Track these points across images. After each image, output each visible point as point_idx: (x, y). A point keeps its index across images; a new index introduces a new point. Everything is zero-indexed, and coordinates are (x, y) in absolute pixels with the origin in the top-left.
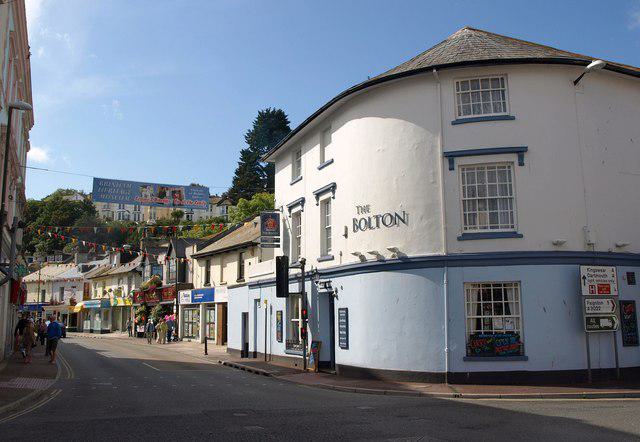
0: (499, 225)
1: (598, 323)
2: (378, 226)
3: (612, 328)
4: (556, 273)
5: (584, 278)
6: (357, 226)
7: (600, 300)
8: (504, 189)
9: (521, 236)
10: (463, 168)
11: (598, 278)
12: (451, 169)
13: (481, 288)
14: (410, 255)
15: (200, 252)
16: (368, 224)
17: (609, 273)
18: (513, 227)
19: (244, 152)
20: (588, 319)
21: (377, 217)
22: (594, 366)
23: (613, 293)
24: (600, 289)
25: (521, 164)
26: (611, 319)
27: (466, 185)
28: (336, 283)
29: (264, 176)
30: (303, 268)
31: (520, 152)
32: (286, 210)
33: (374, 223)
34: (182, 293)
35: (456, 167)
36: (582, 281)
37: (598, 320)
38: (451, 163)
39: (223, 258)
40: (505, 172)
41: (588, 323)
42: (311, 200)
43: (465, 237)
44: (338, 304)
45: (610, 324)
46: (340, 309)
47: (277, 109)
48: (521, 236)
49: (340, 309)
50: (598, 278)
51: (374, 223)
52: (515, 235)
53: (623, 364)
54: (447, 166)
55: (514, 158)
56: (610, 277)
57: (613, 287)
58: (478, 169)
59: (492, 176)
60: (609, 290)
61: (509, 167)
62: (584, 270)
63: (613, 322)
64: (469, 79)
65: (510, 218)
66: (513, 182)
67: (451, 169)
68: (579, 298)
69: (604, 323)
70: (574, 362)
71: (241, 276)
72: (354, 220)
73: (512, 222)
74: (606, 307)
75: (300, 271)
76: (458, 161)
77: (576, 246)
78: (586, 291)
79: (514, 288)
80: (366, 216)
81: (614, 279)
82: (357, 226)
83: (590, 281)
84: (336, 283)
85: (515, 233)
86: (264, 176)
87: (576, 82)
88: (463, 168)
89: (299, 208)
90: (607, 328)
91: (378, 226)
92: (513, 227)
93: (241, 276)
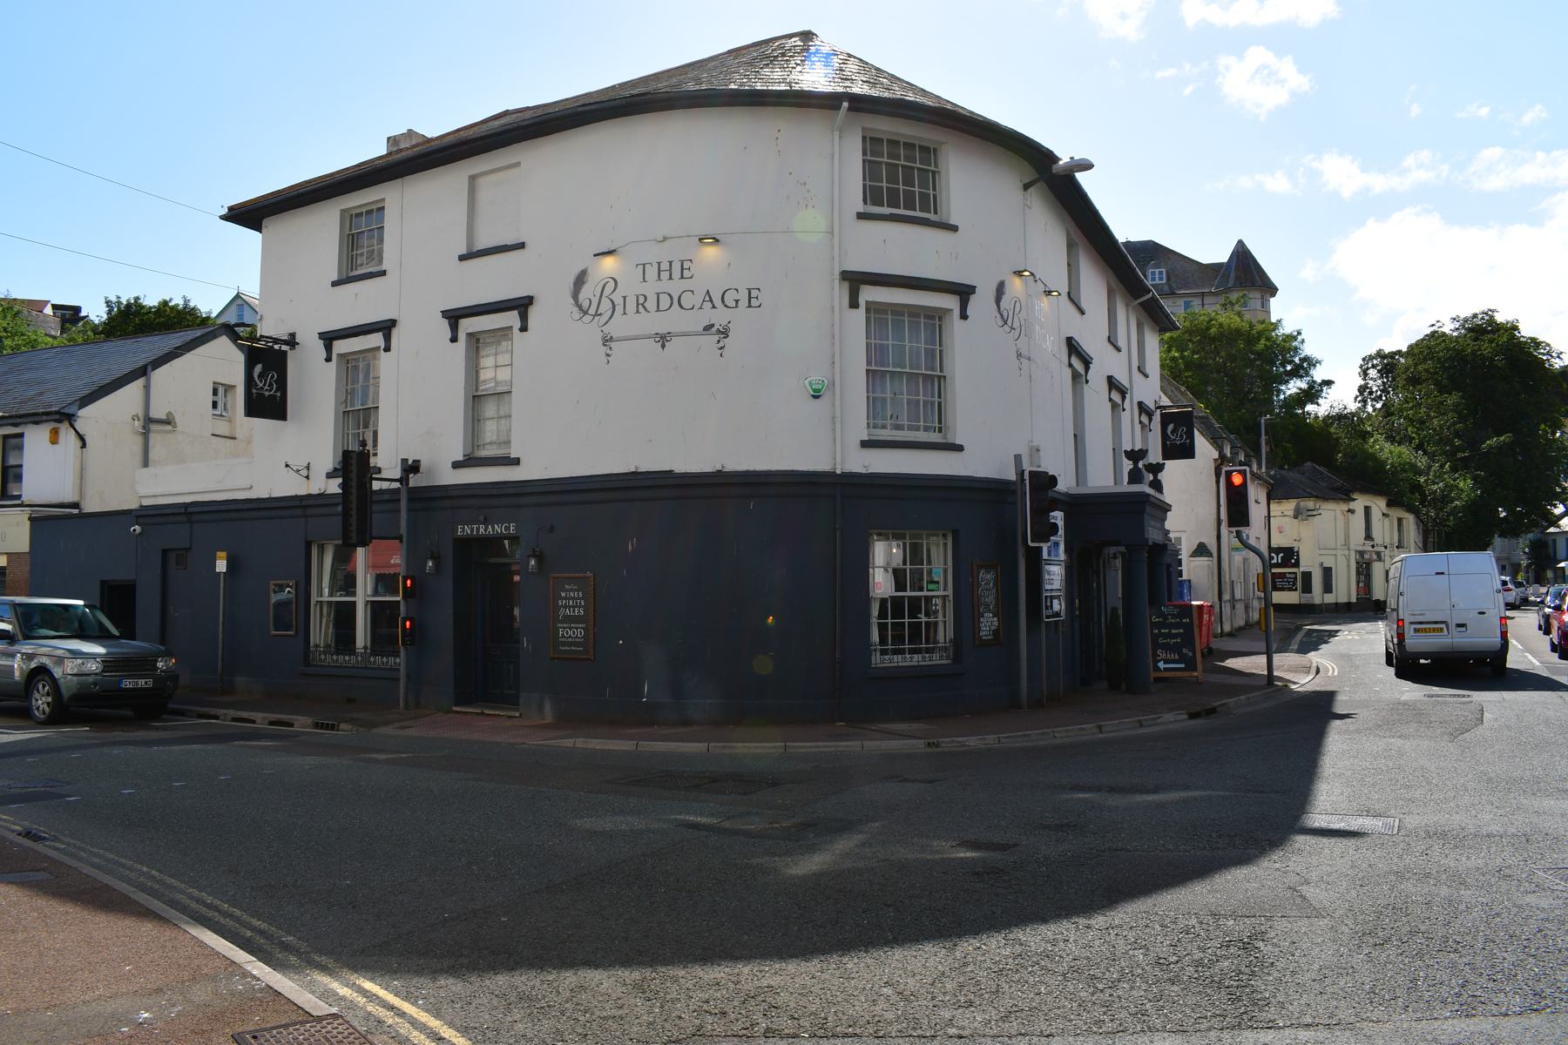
25: (964, 316)
55: (950, 302)
61: (940, 319)
65: (938, 414)
76: (869, 294)
88: (872, 308)
89: (376, 339)
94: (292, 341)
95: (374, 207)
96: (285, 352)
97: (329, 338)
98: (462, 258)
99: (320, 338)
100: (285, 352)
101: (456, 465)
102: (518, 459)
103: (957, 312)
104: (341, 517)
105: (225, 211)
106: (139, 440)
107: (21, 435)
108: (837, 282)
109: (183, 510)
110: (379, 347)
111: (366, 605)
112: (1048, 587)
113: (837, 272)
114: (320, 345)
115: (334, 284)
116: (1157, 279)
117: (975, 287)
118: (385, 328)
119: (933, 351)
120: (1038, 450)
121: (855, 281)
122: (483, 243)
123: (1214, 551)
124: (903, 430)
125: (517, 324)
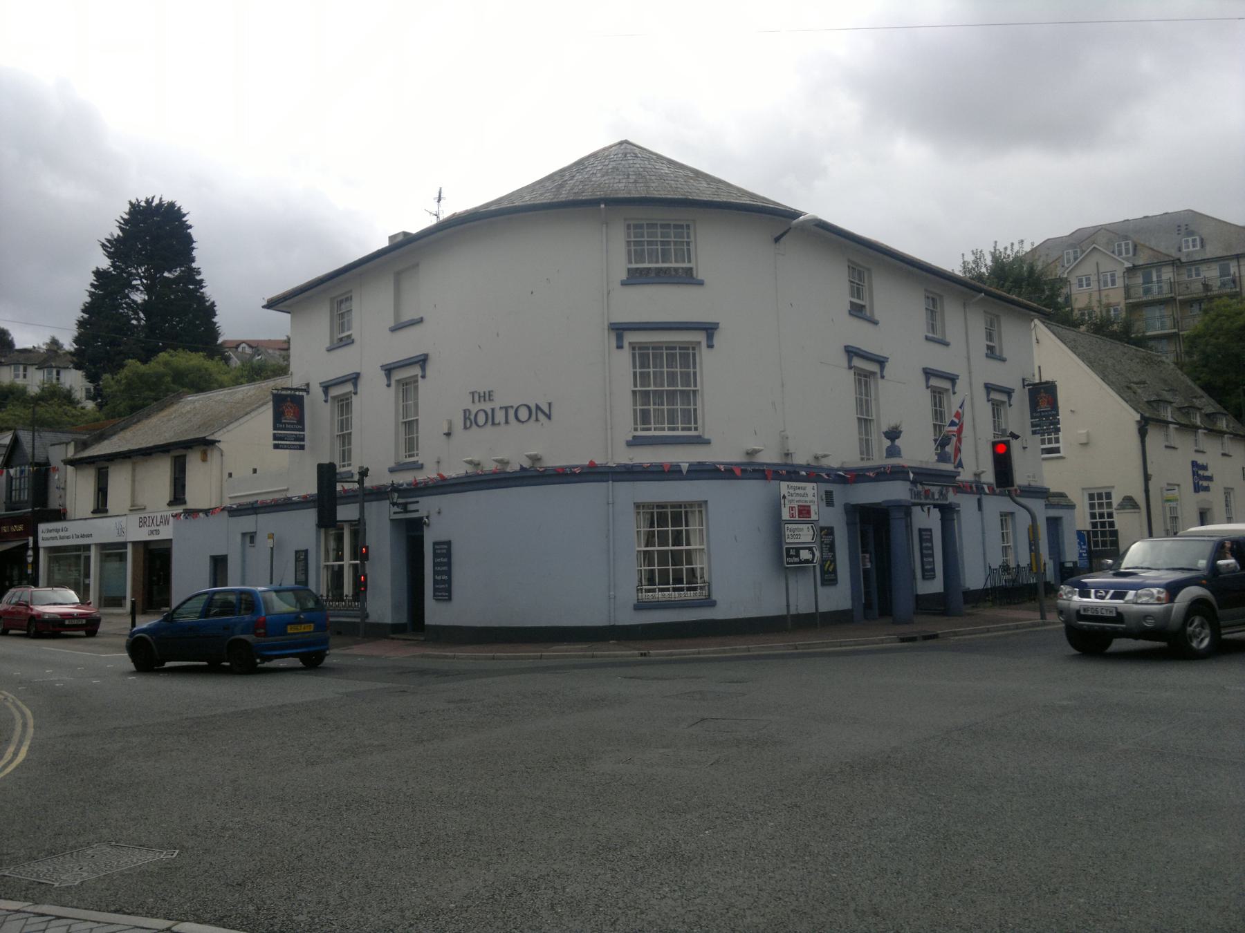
0: (652, 426)
1: (798, 555)
2: (507, 422)
3: (812, 562)
4: (753, 492)
5: (784, 497)
6: (469, 420)
7: (800, 526)
8: (686, 378)
9: (708, 442)
10: (633, 346)
11: (798, 498)
12: (620, 347)
13: (655, 510)
14: (596, 463)
15: (79, 456)
16: (491, 419)
17: (810, 492)
18: (696, 429)
19: (98, 274)
20: (788, 550)
21: (506, 409)
22: (793, 611)
23: (814, 517)
24: (800, 512)
25: (710, 346)
26: (810, 549)
27: (692, 370)
28: (425, 506)
29: (139, 319)
30: (361, 482)
31: (710, 330)
32: (316, 390)
33: (500, 416)
34: (42, 527)
35: (626, 345)
36: (782, 501)
37: (797, 550)
38: (620, 338)
39: (134, 464)
40: (687, 355)
41: (788, 555)
42: (373, 383)
43: (635, 442)
44: (430, 537)
45: (809, 557)
46: (435, 544)
47: (166, 200)
48: (708, 442)
49: (435, 544)
50: (798, 498)
51: (500, 416)
52: (701, 441)
53: (823, 608)
54: (614, 343)
55: (700, 337)
56: (810, 498)
57: (814, 509)
58: (680, 348)
59: (671, 357)
60: (809, 512)
61: (694, 349)
62: (784, 487)
63: (814, 555)
64: (645, 223)
65: (690, 417)
66: (698, 369)
67: (620, 347)
68: (778, 526)
69: (805, 555)
70: (771, 605)
71: (178, 497)
72: (466, 413)
73: (696, 422)
74: (805, 534)
75: (357, 486)
76: (630, 337)
77: (769, 456)
78: (786, 515)
79: (697, 509)
80: (487, 406)
81: (815, 499)
82: (469, 420)
83: (791, 501)
84: (425, 506)
85: (699, 437)
86: (139, 319)
87: (777, 240)
88: (633, 346)
89: (348, 388)
90: (807, 561)
91: (507, 422)
92: (696, 429)
93: (178, 497)
94: (307, 389)
95: (344, 297)
96: (303, 396)
97: (326, 388)
98: (394, 330)
99: (382, 370)
100: (303, 396)
101: (392, 471)
102: (422, 465)
103: (704, 344)
104: (781, 482)
105: (265, 303)
106: (1242, 274)
107: (185, 456)
108: (606, 332)
109: (250, 506)
110: (417, 375)
111: (349, 567)
112: (788, 541)
113: (606, 324)
114: (320, 390)
115: (329, 350)
116: (1123, 245)
117: (718, 324)
118: (420, 361)
119: (688, 374)
120: (787, 438)
121: (619, 330)
122: (406, 318)
123: (1142, 504)
124: (665, 430)
125: (420, 374)
